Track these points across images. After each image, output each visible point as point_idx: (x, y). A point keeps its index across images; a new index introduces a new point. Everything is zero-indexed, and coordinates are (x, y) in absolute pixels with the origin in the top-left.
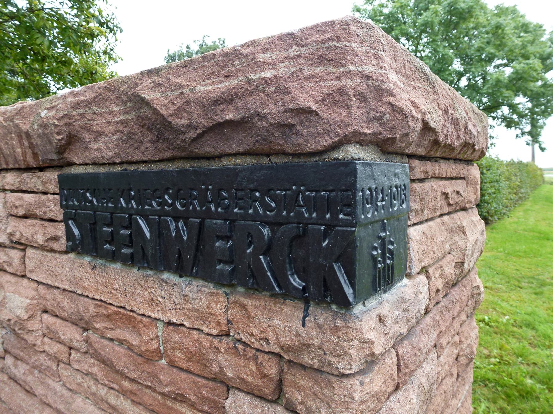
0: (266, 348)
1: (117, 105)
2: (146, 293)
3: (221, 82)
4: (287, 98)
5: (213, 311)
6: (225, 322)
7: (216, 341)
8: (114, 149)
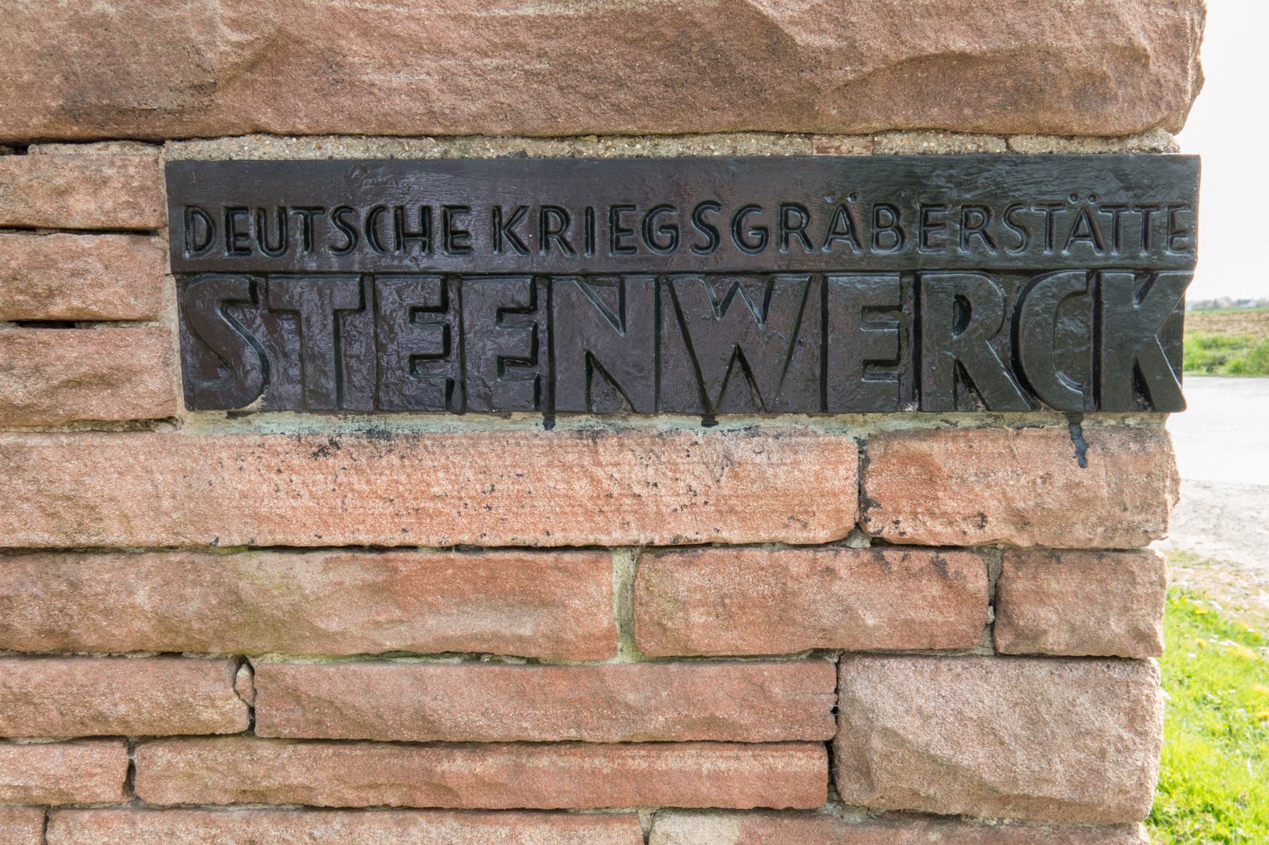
4: (1109, 26)
7: (824, 557)
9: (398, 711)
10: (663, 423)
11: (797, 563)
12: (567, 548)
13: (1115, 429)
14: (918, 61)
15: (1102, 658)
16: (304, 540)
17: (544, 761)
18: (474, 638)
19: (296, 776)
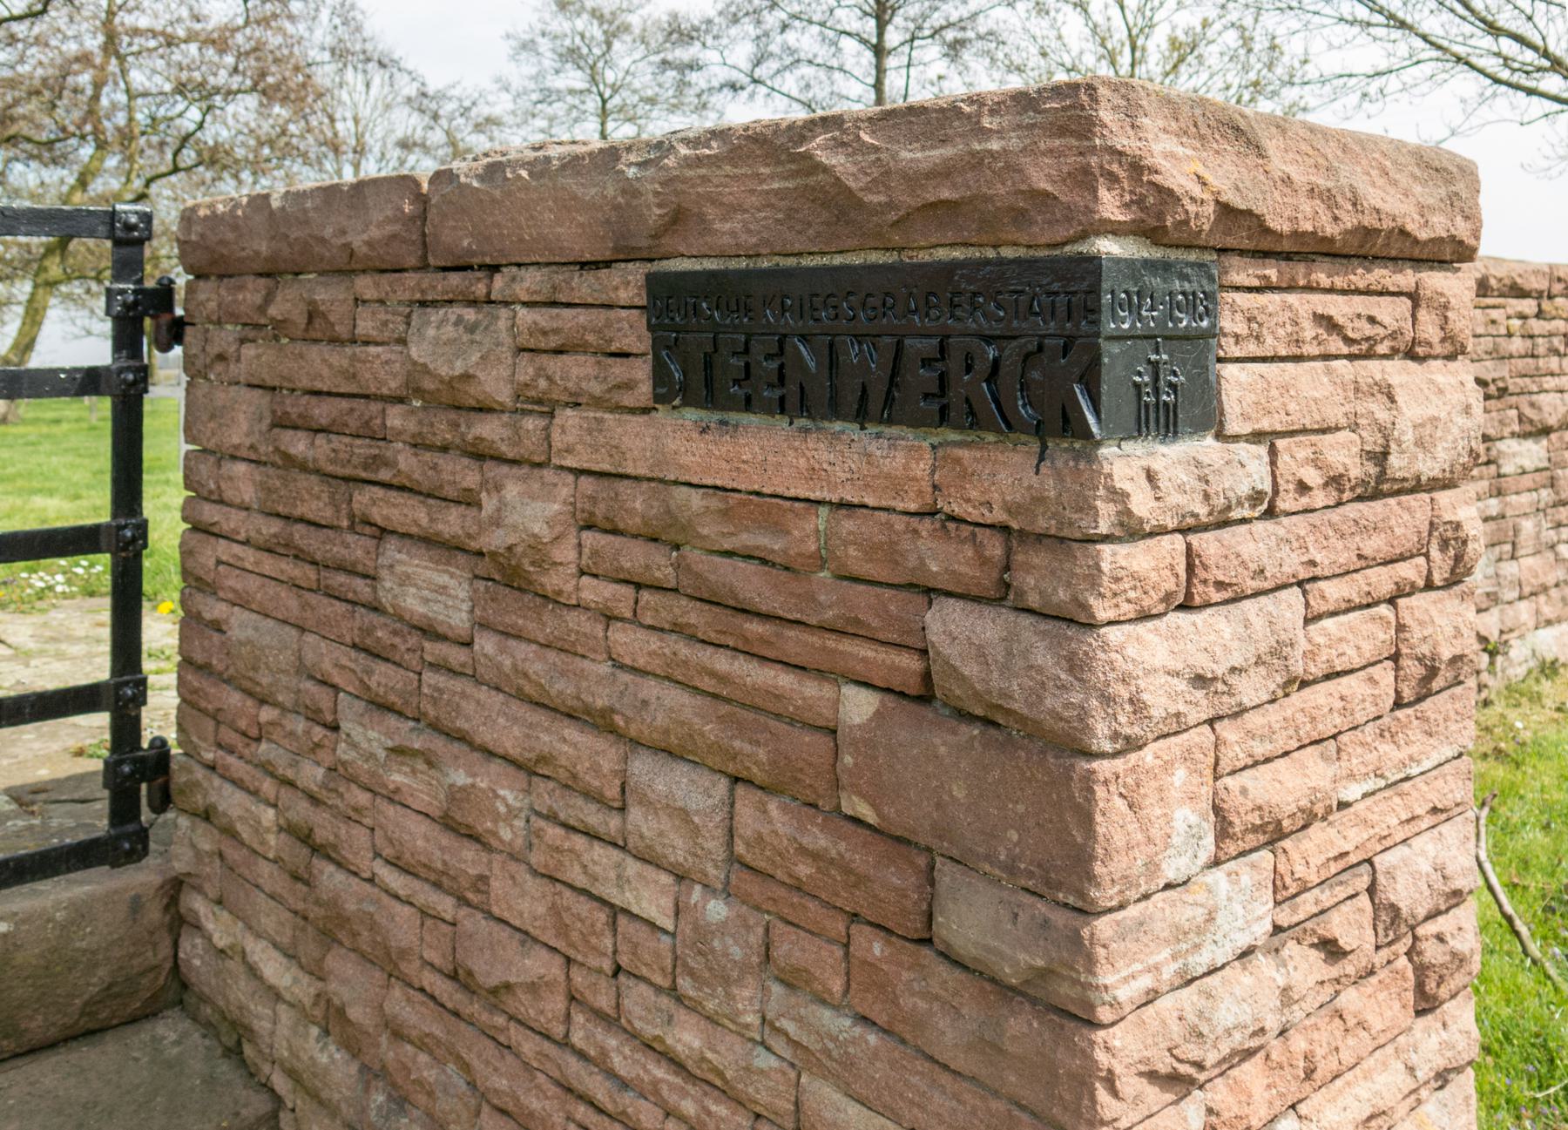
0: (989, 518)
1: (767, 165)
2: (802, 461)
3: (933, 147)
5: (912, 474)
6: (930, 489)
7: (914, 521)
8: (759, 232)
9: (724, 585)
10: (838, 426)
11: (899, 523)
12: (797, 499)
13: (1066, 450)
14: (933, 205)
15: (1064, 619)
16: (695, 480)
17: (791, 633)
18: (758, 548)
19: (693, 619)
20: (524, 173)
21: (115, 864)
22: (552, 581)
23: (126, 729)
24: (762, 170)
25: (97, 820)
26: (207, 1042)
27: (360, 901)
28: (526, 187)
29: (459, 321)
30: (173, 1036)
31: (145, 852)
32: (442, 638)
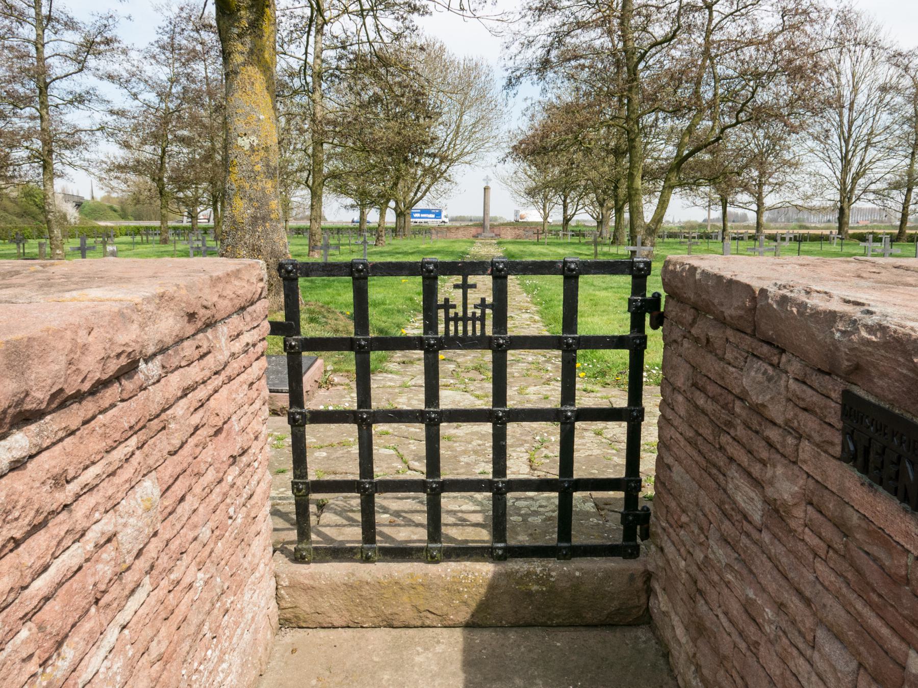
20: (795, 310)
21: (625, 558)
22: (793, 524)
23: (631, 500)
24: (900, 359)
25: (617, 537)
26: (657, 646)
27: (712, 624)
28: (794, 318)
29: (765, 373)
30: (644, 639)
31: (638, 555)
32: (750, 523)
